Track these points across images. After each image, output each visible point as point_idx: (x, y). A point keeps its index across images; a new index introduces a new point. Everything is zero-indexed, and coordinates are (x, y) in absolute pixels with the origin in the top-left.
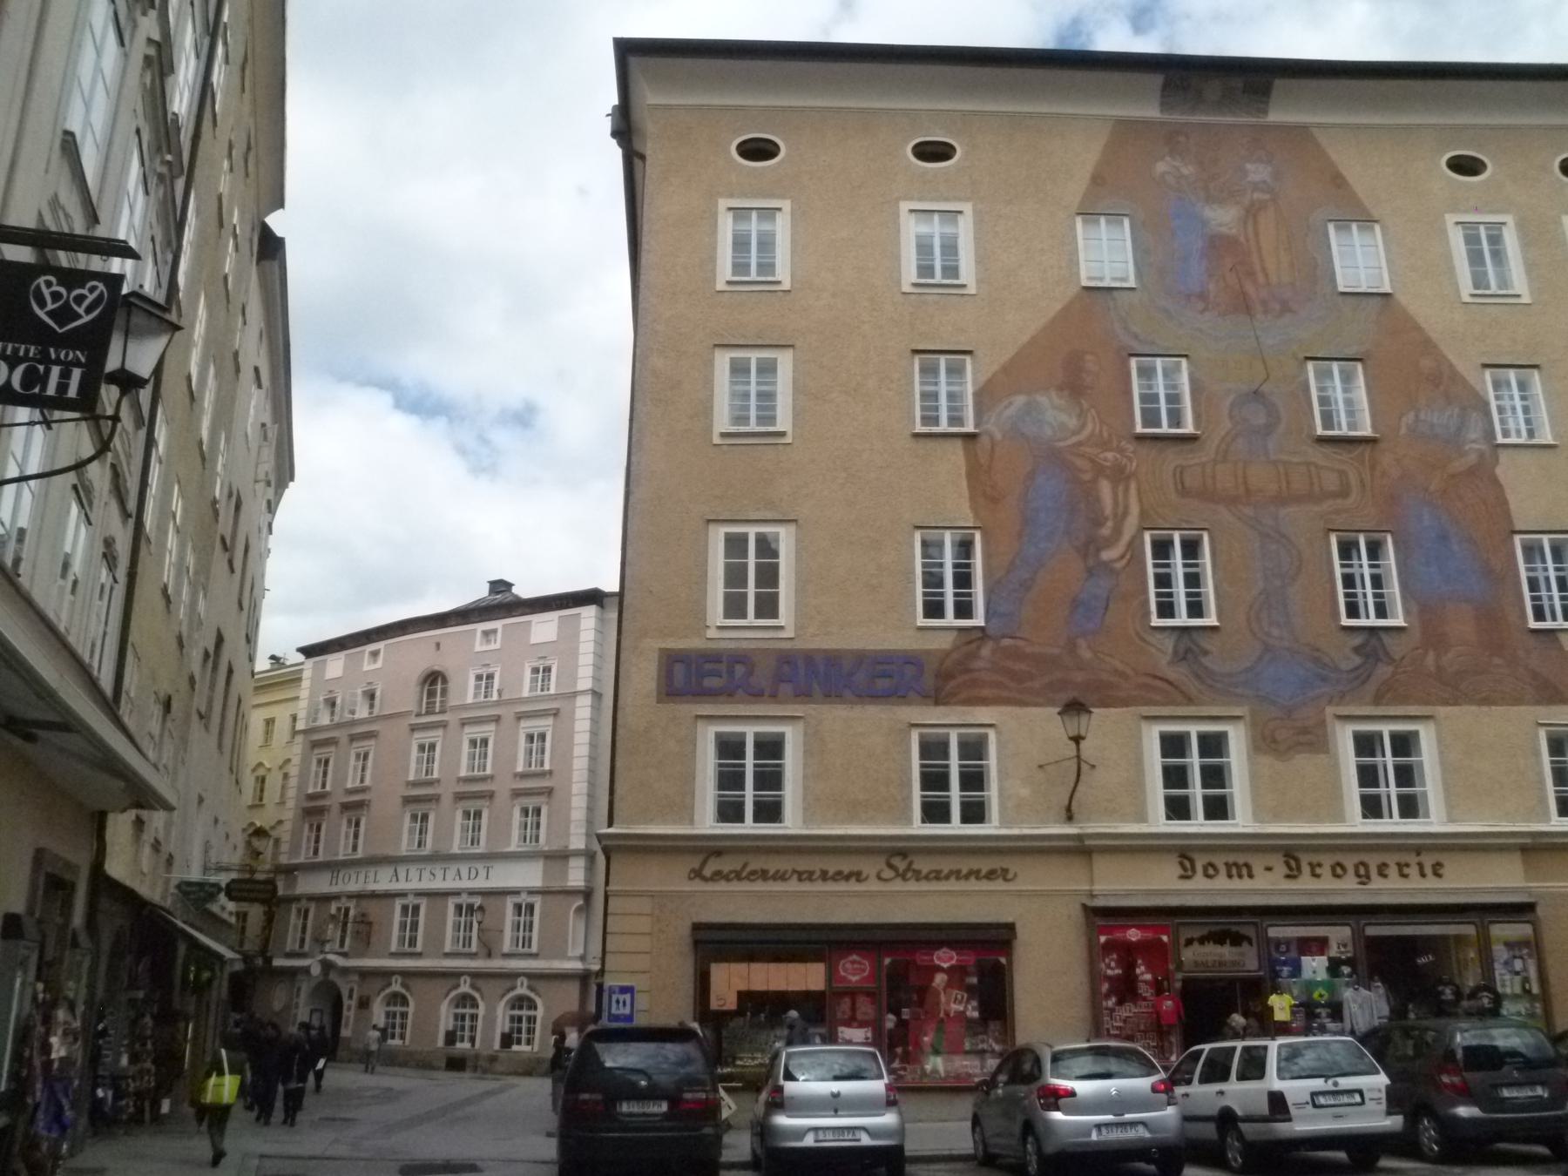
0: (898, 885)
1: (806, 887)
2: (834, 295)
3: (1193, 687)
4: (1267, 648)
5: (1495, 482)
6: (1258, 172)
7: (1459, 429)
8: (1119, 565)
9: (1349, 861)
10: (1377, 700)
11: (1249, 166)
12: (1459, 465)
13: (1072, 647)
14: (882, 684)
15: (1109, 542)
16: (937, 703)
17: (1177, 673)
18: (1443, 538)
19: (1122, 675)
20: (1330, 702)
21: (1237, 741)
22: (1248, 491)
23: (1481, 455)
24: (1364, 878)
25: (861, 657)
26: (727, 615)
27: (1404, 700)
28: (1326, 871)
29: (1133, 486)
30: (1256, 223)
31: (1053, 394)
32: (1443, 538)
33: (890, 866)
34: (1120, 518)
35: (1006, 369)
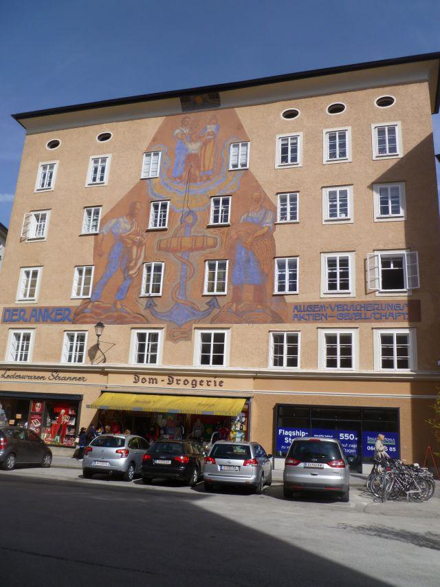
0: (54, 381)
1: (30, 381)
2: (66, 191)
3: (150, 317)
4: (176, 303)
5: (272, 239)
6: (211, 128)
7: (262, 221)
8: (133, 276)
9: (190, 379)
10: (212, 322)
11: (208, 127)
12: (259, 233)
13: (115, 303)
14: (59, 317)
15: (132, 268)
16: (73, 323)
17: (146, 313)
18: (248, 261)
19: (129, 313)
20: (194, 323)
21: (161, 334)
22: (181, 247)
23: (269, 228)
24: (194, 385)
25: (54, 309)
26: (209, 291)
27: (222, 322)
28: (182, 382)
29: (144, 248)
30: (205, 147)
31: (125, 217)
32: (248, 261)
33: (53, 375)
34: (137, 259)
35: (112, 211)
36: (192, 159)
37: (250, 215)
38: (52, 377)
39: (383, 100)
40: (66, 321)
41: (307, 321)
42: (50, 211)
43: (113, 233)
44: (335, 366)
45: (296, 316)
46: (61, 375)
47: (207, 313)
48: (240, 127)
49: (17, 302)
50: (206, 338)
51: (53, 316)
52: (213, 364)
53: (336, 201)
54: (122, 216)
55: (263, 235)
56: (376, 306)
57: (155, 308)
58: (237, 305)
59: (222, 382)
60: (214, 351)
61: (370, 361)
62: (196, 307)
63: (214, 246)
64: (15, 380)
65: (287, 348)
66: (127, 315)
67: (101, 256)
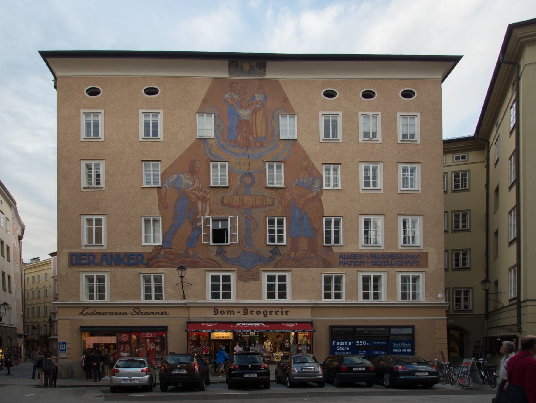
0: (137, 316)
1: (112, 317)
9: (262, 310)
10: (275, 266)
11: (256, 95)
12: (310, 196)
13: (187, 250)
16: (148, 267)
18: (302, 218)
19: (202, 259)
21: (233, 277)
23: (318, 192)
25: (126, 254)
27: (283, 266)
28: (255, 313)
30: (256, 115)
32: (302, 218)
36: (243, 124)
37: (301, 180)
38: (134, 313)
39: (406, 92)
40: (122, 264)
41: (350, 266)
42: (104, 162)
43: (175, 187)
44: (274, 298)
45: (341, 262)
46: (143, 311)
47: (271, 259)
48: (286, 100)
49: (83, 248)
50: (271, 279)
51: (126, 260)
52: (223, 298)
53: (221, 176)
54: (183, 173)
55: (313, 198)
56: (399, 256)
57: (225, 255)
58: (295, 254)
59: (287, 312)
60: (277, 287)
61: (352, 294)
62: (261, 254)
63: (273, 205)
64: (95, 317)
65: (332, 286)
66: (199, 260)
67: (166, 208)
